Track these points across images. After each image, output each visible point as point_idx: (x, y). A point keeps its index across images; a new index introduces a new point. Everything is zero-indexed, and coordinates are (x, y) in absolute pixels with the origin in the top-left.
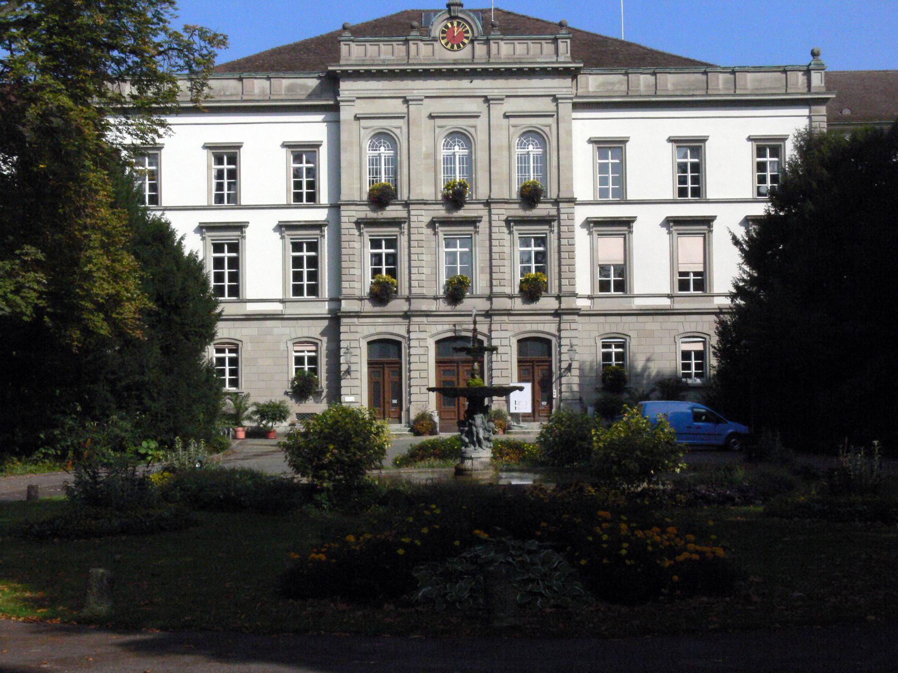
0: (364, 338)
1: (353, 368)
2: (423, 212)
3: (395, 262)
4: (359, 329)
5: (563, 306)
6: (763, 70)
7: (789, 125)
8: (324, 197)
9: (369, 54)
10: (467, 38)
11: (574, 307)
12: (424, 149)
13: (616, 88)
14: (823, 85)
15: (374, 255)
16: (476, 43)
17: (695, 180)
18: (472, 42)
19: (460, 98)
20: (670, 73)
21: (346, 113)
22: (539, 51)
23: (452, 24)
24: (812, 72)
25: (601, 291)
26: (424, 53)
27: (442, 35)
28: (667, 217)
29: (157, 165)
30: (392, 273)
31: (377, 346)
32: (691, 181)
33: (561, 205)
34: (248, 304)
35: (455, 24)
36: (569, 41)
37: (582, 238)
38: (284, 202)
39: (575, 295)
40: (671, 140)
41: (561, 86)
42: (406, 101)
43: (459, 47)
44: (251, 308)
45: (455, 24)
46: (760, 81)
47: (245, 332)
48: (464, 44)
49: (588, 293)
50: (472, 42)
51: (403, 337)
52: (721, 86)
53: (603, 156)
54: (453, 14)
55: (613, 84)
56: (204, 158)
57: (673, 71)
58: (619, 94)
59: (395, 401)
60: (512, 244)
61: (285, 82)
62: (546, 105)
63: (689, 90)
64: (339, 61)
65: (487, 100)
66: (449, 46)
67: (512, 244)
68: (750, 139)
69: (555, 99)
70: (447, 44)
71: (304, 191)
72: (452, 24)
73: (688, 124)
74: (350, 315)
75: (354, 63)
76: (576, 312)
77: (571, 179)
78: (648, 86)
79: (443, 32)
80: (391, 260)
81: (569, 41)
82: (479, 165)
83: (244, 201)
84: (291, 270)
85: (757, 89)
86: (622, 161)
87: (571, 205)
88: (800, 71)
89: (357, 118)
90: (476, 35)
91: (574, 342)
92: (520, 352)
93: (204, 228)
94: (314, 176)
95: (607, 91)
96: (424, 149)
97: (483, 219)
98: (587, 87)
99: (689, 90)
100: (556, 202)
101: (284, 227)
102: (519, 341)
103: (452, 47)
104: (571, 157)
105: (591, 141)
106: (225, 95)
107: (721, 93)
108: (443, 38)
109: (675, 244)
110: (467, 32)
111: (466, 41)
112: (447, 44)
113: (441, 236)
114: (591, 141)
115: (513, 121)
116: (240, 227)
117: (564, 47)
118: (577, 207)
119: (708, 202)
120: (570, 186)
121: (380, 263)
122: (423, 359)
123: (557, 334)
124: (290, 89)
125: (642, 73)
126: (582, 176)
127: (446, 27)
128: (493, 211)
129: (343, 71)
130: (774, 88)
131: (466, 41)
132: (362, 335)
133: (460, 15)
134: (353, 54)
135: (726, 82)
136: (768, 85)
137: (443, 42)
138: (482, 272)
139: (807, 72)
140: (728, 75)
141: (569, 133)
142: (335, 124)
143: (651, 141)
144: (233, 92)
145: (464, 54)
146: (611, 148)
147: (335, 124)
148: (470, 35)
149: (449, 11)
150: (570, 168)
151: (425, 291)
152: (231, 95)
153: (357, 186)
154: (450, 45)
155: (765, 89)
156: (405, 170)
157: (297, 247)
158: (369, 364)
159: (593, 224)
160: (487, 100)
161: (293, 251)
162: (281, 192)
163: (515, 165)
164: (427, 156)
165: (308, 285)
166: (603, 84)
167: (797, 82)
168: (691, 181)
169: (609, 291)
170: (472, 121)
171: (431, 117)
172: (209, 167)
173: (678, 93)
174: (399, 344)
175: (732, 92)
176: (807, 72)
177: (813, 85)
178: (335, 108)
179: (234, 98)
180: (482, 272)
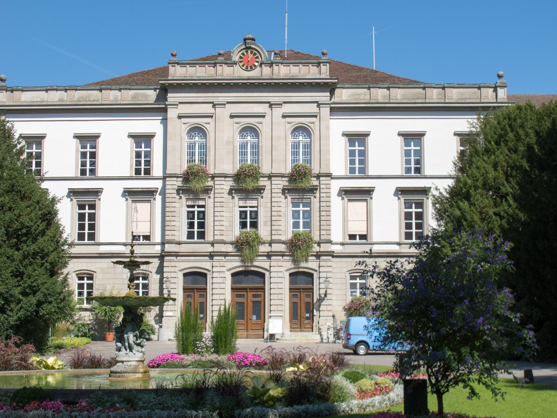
0: (181, 271)
1: (172, 291)
2: (224, 182)
3: (310, 217)
4: (177, 264)
5: (322, 250)
6: (464, 86)
7: (465, 124)
8: (157, 170)
9: (189, 73)
10: (257, 62)
11: (330, 250)
12: (226, 138)
13: (362, 98)
14: (506, 97)
15: (294, 212)
16: (263, 65)
17: (362, 162)
18: (261, 66)
19: (251, 104)
20: (399, 88)
21: (172, 113)
22: (307, 72)
23: (247, 52)
24: (498, 88)
25: (78, 240)
26: (226, 72)
27: (240, 60)
28: (397, 188)
29: (150, 148)
30: (307, 225)
31: (190, 278)
32: (88, 163)
33: (321, 178)
34: (101, 246)
35: (249, 51)
36: (328, 65)
37: (337, 203)
38: (73, 175)
39: (330, 242)
40: (400, 134)
41: (323, 96)
42: (214, 106)
43: (251, 67)
44: (103, 249)
45: (249, 51)
46: (462, 94)
47: (98, 265)
48: (255, 66)
49: (341, 240)
50: (261, 66)
51: (316, 271)
52: (435, 97)
53: (407, 144)
54: (247, 46)
55: (360, 94)
56: (74, 145)
57: (402, 86)
58: (363, 101)
59: (308, 315)
60: (287, 206)
61: (132, 92)
62: (313, 109)
63: (412, 99)
64: (168, 76)
65: (271, 105)
66: (249, 69)
67: (287, 206)
68: (456, 134)
69: (319, 105)
70: (243, 66)
71: (142, 169)
72: (247, 52)
73: (87, 126)
74: (170, 254)
75: (282, 77)
76: (332, 254)
77: (328, 160)
78: (384, 96)
79: (241, 58)
80: (306, 216)
81: (328, 65)
82: (264, 150)
83: (371, 173)
84: (404, 222)
85: (460, 99)
86: (421, 148)
87: (329, 178)
88: (490, 87)
89: (180, 117)
90: (263, 60)
91: (329, 275)
92: (291, 282)
93: (73, 193)
94: (420, 156)
95: (355, 99)
96: (226, 138)
97: (266, 188)
98: (341, 97)
99: (412, 99)
100: (318, 177)
101: (401, 192)
102: (291, 275)
103: (247, 68)
104: (329, 145)
105: (345, 135)
106: (89, 100)
107: (435, 101)
108: (241, 62)
109: (346, 207)
110: (257, 58)
111: (256, 64)
112: (243, 66)
113: (289, 198)
114: (345, 135)
115: (288, 120)
116: (96, 192)
117: (325, 69)
118: (333, 181)
119: (426, 177)
120: (328, 165)
121: (193, 218)
122: (222, 286)
123: (317, 269)
124: (134, 97)
125: (379, 88)
126: (336, 157)
127: (243, 54)
128: (273, 182)
129: (170, 84)
130: (469, 99)
131: (256, 64)
132: (227, 268)
133: (252, 46)
134: (177, 73)
135: (438, 94)
136: (468, 97)
137: (241, 64)
138: (265, 224)
139: (495, 89)
140: (441, 90)
141: (328, 128)
142: (165, 121)
143: (384, 136)
144: (96, 98)
145: (255, 73)
146: (357, 139)
147: (165, 121)
148: (259, 60)
149: (245, 43)
150: (328, 152)
151: (224, 238)
152: (94, 101)
153: (179, 165)
154: (245, 66)
155: (465, 99)
156: (212, 153)
157: (82, 207)
158: (184, 289)
159: (346, 193)
160: (271, 105)
161: (293, 207)
162: (126, 167)
163: (290, 150)
164: (228, 143)
165: (416, 232)
166: (353, 95)
167: (488, 95)
168: (88, 163)
169: (194, 239)
170: (313, 119)
171: (232, 117)
172: (77, 150)
173: (405, 101)
174: (311, 275)
175: (495, 101)
176: (495, 89)
177: (498, 97)
178: (164, 110)
179: (96, 103)
180: (265, 224)
